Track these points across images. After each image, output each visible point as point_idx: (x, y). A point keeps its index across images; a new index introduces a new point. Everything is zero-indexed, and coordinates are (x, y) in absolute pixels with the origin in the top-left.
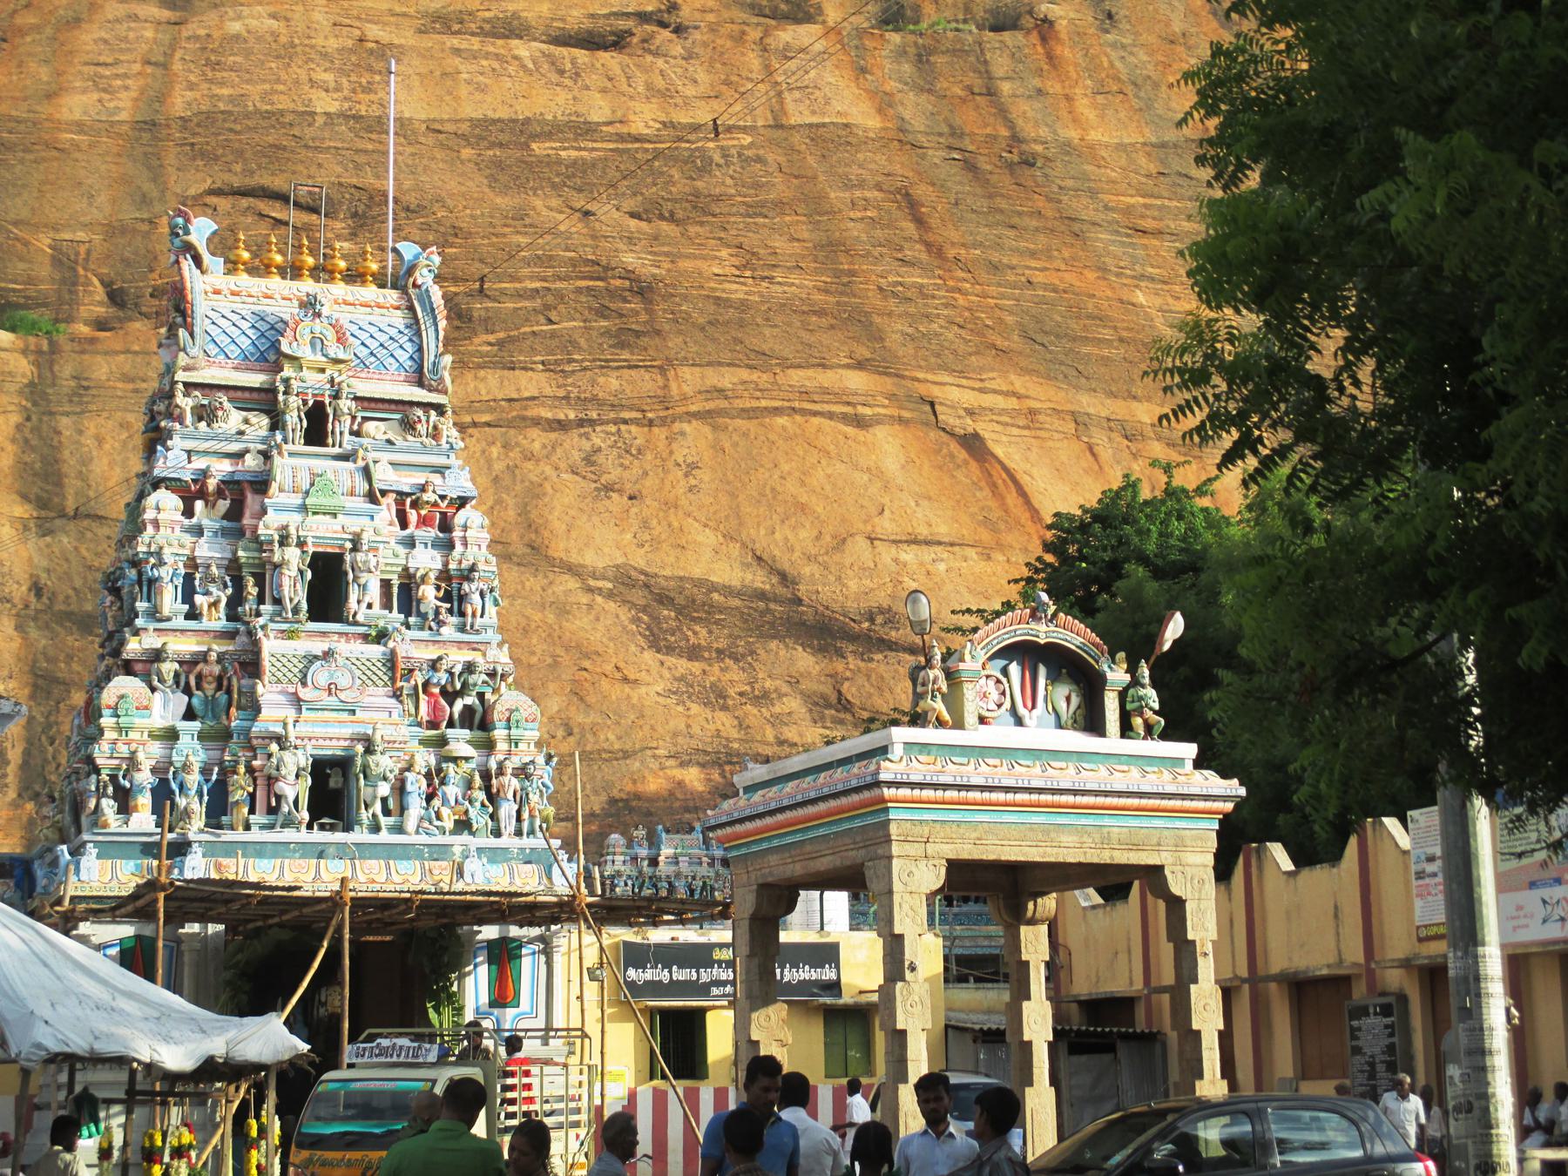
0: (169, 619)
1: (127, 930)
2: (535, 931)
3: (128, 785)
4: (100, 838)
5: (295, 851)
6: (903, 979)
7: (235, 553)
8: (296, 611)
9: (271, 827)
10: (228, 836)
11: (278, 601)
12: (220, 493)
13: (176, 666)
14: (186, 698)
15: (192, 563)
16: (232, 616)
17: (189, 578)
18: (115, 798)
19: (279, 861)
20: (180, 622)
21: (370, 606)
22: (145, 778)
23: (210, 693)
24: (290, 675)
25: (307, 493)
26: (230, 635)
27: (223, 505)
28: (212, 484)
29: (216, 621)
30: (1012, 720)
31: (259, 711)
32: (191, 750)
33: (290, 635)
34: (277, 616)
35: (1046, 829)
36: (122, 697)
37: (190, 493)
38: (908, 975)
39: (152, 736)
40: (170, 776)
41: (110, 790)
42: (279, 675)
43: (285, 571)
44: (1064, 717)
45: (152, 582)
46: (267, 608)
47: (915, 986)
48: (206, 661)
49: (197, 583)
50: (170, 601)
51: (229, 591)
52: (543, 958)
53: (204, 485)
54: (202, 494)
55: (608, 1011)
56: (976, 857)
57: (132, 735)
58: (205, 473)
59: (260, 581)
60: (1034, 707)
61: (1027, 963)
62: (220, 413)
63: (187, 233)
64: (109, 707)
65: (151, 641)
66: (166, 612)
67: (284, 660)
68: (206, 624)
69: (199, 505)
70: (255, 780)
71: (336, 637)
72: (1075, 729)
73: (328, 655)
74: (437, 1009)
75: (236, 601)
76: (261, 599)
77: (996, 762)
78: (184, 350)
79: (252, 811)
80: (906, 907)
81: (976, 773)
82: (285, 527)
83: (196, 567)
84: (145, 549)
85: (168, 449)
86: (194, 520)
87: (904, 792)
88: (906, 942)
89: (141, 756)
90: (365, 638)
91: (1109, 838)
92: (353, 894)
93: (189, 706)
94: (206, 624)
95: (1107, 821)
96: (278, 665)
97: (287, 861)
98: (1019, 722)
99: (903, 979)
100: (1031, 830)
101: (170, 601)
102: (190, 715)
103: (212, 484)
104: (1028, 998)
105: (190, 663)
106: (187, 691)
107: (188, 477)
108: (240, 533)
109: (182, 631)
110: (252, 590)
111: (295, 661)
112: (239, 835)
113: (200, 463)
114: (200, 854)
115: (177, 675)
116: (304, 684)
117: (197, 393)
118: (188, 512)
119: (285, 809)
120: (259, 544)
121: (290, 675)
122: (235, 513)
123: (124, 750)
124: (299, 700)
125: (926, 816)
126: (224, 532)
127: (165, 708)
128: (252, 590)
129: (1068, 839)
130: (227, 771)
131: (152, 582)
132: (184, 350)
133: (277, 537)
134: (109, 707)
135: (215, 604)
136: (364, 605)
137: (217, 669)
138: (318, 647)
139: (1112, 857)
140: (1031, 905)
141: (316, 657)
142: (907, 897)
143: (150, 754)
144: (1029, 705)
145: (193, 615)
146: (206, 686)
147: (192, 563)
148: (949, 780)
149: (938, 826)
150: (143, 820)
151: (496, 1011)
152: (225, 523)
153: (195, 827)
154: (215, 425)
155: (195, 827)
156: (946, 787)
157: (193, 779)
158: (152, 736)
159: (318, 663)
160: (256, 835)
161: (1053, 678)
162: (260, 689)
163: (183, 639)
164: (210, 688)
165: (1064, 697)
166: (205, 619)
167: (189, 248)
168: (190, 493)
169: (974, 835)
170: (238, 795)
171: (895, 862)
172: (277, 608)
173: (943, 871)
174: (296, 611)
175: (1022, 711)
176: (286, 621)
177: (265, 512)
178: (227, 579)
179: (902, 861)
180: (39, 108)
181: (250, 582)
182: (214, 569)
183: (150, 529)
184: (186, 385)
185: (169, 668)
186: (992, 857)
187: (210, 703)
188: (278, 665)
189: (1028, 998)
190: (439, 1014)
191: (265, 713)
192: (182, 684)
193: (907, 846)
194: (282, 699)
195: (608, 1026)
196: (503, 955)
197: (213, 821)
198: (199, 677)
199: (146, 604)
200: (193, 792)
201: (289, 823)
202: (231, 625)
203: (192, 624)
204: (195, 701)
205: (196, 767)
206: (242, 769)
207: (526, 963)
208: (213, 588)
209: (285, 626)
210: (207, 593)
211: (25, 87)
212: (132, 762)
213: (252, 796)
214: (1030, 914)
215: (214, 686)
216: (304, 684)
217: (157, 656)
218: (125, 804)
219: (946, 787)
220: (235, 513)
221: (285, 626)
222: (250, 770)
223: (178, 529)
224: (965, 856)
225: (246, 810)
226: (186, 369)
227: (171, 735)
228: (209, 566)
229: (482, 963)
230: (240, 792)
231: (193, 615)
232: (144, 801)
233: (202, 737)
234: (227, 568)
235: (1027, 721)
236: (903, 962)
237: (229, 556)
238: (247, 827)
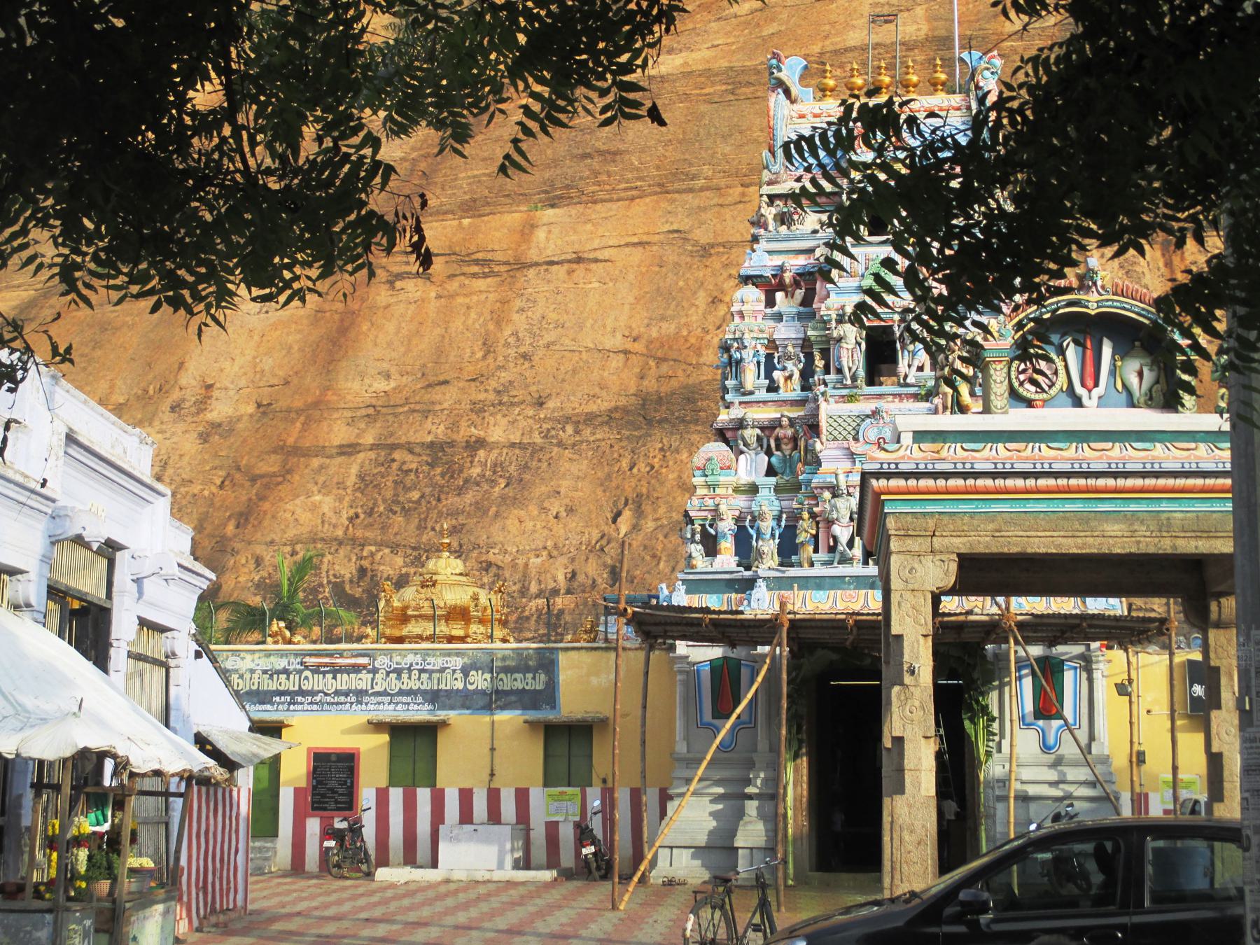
0: (751, 393)
1: (716, 652)
2: (1077, 649)
3: (712, 531)
4: (691, 577)
5: (849, 583)
6: (902, 684)
7: (805, 333)
8: (854, 378)
9: (830, 563)
10: (792, 572)
11: (839, 371)
12: (796, 284)
13: (758, 431)
14: (766, 458)
15: (772, 344)
16: (804, 388)
17: (769, 357)
18: (702, 542)
19: (832, 592)
20: (762, 395)
21: (921, 369)
22: (727, 526)
23: (787, 453)
24: (844, 433)
25: (863, 276)
26: (801, 403)
27: (800, 293)
28: (788, 277)
29: (791, 391)
30: (1069, 401)
31: (819, 463)
32: (768, 503)
33: (851, 398)
34: (840, 384)
35: (1084, 519)
36: (709, 459)
37: (771, 286)
38: (907, 679)
39: (737, 490)
40: (747, 524)
41: (698, 537)
42: (835, 433)
43: (844, 345)
44: (1136, 394)
45: (739, 362)
46: (832, 377)
47: (917, 692)
48: (781, 426)
49: (776, 361)
50: (751, 377)
51: (801, 366)
52: (1084, 675)
53: (782, 278)
54: (781, 286)
55: (1179, 723)
56: (994, 550)
57: (718, 491)
58: (781, 268)
59: (825, 354)
60: (1096, 385)
61: (1217, 669)
62: (796, 217)
63: (780, 70)
64: (699, 469)
65: (736, 412)
66: (749, 386)
67: (840, 421)
68: (783, 394)
69: (779, 296)
70: (818, 523)
71: (890, 399)
72: (1149, 407)
73: (875, 414)
74: (972, 720)
75: (807, 374)
76: (827, 370)
77: (1021, 446)
78: (767, 167)
79: (816, 551)
80: (906, 606)
81: (985, 457)
82: (843, 307)
83: (776, 348)
84: (731, 336)
85: (754, 251)
86: (776, 309)
87: (895, 483)
88: (906, 644)
89: (723, 508)
90: (916, 397)
91: (1169, 525)
92: (791, 616)
93: (770, 464)
94: (783, 394)
95: (1164, 506)
96: (835, 424)
97: (839, 592)
98: (1078, 402)
99: (902, 684)
100: (1064, 518)
101: (751, 377)
102: (771, 471)
103: (788, 277)
104: (1219, 707)
105: (769, 428)
106: (769, 453)
107: (768, 273)
108: (812, 315)
109: (765, 402)
110: (819, 363)
111: (849, 420)
112: (806, 571)
113: (777, 261)
114: (764, 588)
115: (759, 439)
116: (856, 439)
117: (778, 202)
118: (770, 302)
119: (840, 548)
120: (825, 323)
121: (844, 433)
122: (807, 301)
123: (710, 503)
124: (853, 454)
125: (930, 508)
126: (800, 317)
127: (750, 467)
128: (819, 363)
129: (1114, 528)
130: (795, 517)
131: (739, 362)
132: (767, 167)
133: (834, 316)
134: (699, 469)
135: (790, 377)
136: (914, 369)
137: (789, 432)
138: (867, 407)
139: (1174, 547)
140: (1214, 607)
141: (868, 416)
142: (908, 595)
143: (732, 506)
144: (1090, 383)
145: (773, 388)
146: (784, 447)
147: (772, 344)
148: (948, 467)
149: (946, 518)
150: (727, 560)
151: (1041, 723)
152: (801, 309)
153: (768, 564)
154: (793, 228)
155: (768, 564)
156: (947, 475)
157: (767, 525)
158: (737, 490)
159: (868, 421)
160: (818, 571)
161: (1122, 352)
162: (818, 446)
163: (766, 409)
164: (787, 448)
165: (1136, 373)
166: (781, 391)
167: (780, 84)
168: (771, 286)
169: (991, 526)
170: (802, 537)
171: (894, 558)
172: (839, 376)
173: (954, 567)
174: (854, 378)
175: (1079, 389)
176: (845, 387)
177: (828, 296)
178: (802, 355)
179: (901, 557)
180: (987, 26)
181: (817, 356)
182: (790, 348)
183: (737, 319)
184: (769, 196)
185: (750, 434)
186: (1015, 550)
187: (788, 462)
188: (835, 424)
189: (1219, 707)
190: (975, 724)
191: (825, 466)
192: (765, 446)
193: (909, 541)
194: (839, 453)
195: (1181, 737)
196: (1049, 671)
197: (786, 560)
198: (777, 440)
199: (734, 382)
200: (768, 536)
201: (845, 560)
202: (804, 393)
203: (772, 396)
204: (773, 460)
205: (769, 516)
206: (806, 515)
207: (1068, 676)
208: (789, 365)
209: (845, 392)
210: (784, 369)
211: (979, 12)
212: (717, 515)
213: (816, 537)
214: (1214, 616)
215: (789, 446)
216: (856, 439)
217: (741, 424)
218: (711, 547)
219: (947, 475)
220: (807, 301)
221: (845, 392)
222: (813, 516)
223: (760, 318)
224: (981, 549)
225: (811, 548)
226: (770, 183)
227: (753, 489)
228: (786, 346)
229: (1026, 675)
230: (804, 534)
231: (773, 388)
232: (727, 544)
233: (778, 489)
234: (802, 347)
235: (1085, 400)
236: (901, 664)
237: (802, 336)
238: (812, 564)
